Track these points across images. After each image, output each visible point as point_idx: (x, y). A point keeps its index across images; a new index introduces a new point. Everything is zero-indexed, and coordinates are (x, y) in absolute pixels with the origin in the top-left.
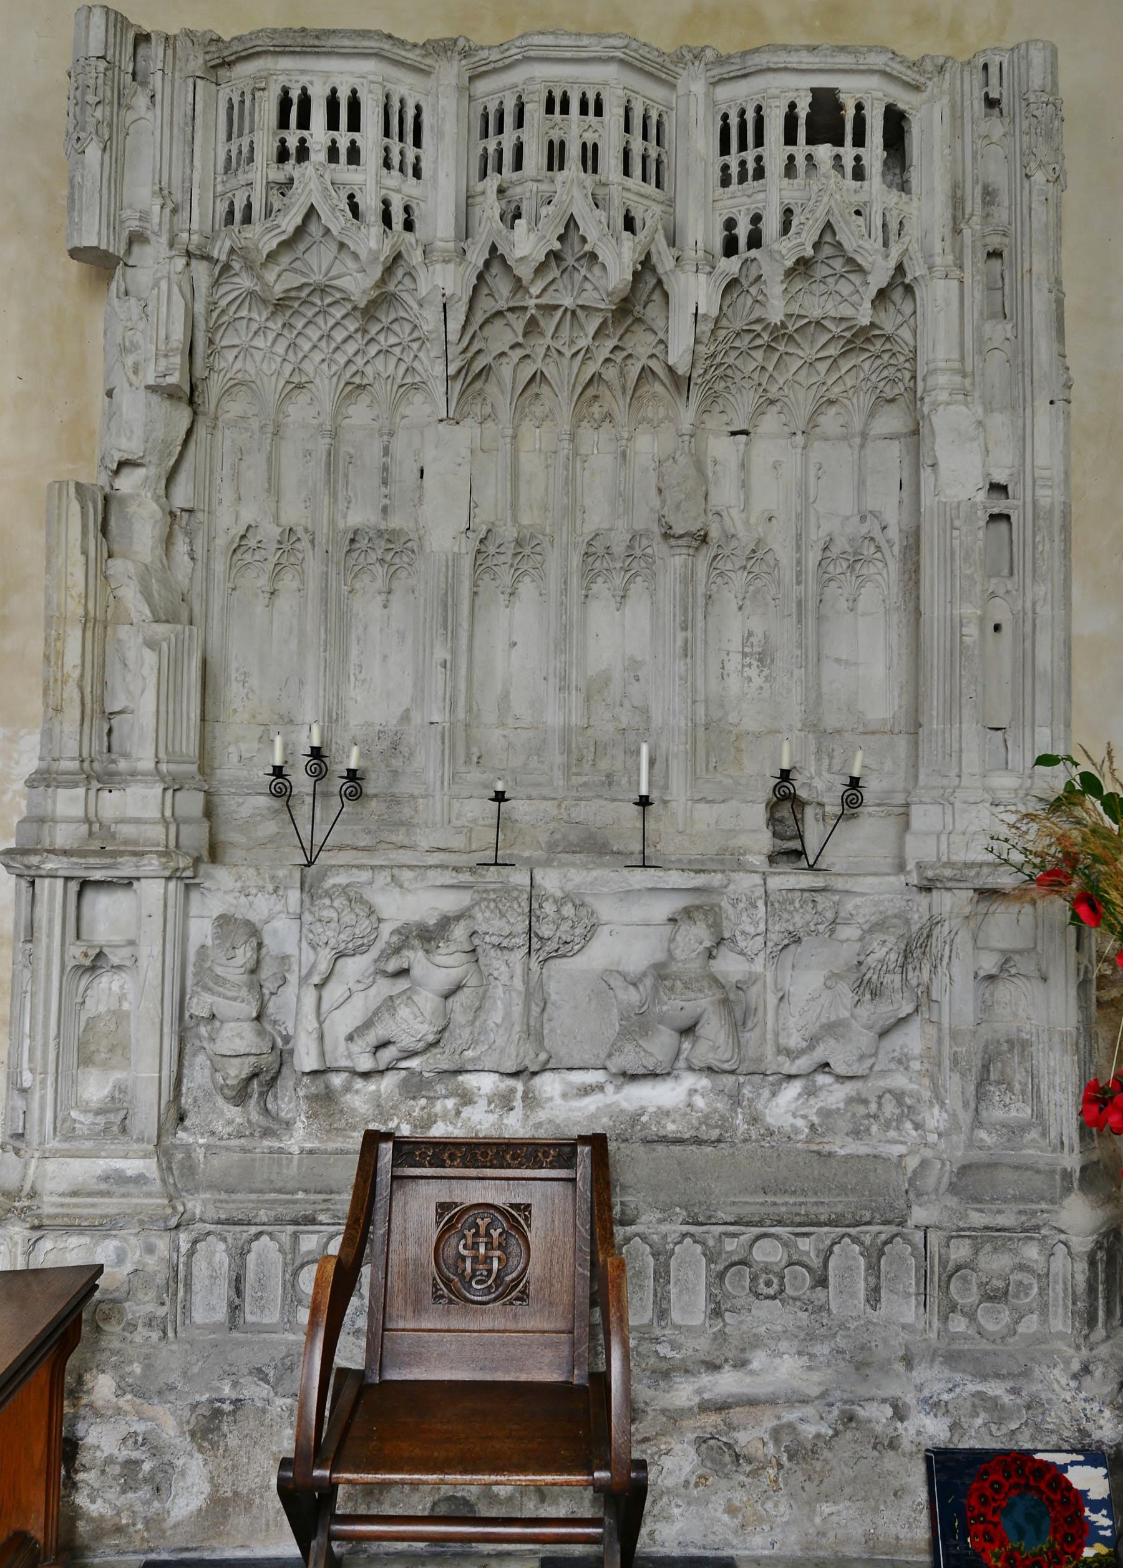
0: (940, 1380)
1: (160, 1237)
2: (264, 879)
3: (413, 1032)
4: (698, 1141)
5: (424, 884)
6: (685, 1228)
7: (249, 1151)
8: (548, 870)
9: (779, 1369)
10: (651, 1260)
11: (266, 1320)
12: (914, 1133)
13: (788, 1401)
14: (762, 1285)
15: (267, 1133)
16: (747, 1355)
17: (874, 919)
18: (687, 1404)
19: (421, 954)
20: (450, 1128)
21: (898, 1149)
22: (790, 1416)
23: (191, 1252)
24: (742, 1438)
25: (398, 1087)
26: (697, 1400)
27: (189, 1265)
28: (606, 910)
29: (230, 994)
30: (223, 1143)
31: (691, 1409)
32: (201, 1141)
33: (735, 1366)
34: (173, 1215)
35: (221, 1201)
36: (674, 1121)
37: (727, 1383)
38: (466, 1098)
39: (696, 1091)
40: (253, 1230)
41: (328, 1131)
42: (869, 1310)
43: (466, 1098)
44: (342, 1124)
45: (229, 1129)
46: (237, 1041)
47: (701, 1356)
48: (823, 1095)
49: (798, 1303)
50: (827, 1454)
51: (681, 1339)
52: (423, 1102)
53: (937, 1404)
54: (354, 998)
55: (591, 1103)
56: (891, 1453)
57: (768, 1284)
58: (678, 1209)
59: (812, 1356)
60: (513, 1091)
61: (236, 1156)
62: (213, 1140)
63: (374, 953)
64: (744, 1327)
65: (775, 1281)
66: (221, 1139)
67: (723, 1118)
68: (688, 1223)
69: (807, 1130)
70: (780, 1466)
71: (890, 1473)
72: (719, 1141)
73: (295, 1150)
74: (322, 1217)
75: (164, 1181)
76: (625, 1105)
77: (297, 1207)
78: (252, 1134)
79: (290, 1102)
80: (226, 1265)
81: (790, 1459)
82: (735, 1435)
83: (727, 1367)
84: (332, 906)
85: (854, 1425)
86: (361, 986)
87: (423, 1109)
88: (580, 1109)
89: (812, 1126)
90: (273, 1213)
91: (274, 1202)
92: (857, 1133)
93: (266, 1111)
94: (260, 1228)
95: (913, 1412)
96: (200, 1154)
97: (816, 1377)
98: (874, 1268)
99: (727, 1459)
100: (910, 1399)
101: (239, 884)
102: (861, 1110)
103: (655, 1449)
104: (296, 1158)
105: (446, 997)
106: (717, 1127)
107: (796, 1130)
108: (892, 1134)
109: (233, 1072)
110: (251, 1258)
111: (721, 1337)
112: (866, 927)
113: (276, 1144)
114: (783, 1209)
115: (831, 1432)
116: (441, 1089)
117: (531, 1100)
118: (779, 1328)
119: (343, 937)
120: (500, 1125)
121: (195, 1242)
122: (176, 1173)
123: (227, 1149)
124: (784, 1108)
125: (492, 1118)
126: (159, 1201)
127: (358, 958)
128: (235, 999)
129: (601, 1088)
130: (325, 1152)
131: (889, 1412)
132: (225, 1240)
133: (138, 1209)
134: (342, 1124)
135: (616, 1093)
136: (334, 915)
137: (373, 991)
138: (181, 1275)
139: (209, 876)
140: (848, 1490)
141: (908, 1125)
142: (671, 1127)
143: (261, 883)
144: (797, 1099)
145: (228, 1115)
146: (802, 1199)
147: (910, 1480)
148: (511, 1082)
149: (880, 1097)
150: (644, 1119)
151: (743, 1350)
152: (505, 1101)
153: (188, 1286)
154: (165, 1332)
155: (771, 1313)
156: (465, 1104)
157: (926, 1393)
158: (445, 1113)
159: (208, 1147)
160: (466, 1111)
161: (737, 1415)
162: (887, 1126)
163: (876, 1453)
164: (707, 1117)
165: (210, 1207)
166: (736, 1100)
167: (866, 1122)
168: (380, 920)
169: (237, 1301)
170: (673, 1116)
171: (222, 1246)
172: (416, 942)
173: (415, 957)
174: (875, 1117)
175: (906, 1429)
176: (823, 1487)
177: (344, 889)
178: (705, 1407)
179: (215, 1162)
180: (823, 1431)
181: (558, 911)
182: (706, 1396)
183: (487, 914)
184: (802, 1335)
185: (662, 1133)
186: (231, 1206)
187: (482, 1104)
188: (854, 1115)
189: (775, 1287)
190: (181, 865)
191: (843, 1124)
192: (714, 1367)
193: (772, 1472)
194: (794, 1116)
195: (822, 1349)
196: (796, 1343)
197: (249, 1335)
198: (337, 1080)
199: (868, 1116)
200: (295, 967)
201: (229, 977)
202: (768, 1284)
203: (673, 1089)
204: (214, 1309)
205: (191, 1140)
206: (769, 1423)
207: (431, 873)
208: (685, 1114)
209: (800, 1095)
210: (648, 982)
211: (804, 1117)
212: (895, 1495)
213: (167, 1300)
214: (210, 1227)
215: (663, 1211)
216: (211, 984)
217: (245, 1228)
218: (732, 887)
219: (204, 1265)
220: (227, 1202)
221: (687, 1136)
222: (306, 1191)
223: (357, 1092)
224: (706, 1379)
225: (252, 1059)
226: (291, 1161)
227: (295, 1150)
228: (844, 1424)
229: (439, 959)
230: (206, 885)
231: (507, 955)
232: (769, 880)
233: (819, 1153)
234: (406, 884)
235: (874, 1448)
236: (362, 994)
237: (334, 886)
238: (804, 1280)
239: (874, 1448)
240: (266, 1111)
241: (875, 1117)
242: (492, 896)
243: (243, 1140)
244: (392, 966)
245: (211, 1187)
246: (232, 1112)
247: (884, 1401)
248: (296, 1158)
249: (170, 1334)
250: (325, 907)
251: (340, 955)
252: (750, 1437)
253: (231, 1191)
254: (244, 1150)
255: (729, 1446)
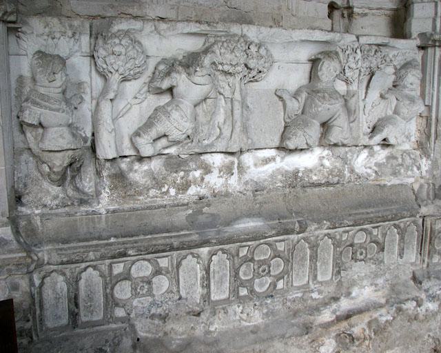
0: (436, 285)
1: (22, 278)
2: (64, 26)
3: (181, 128)
4: (328, 184)
5: (175, 32)
6: (327, 231)
7: (73, 215)
8: (251, 26)
9: (364, 293)
10: (308, 251)
11: (95, 319)
12: (418, 172)
13: (374, 308)
14: (358, 255)
15: (82, 202)
16: (350, 290)
17: (402, 63)
18: (330, 319)
19: (184, 76)
20: (199, 189)
21: (411, 180)
22: (376, 315)
23: (42, 284)
24: (356, 331)
25: (164, 165)
26: (334, 317)
27: (40, 293)
28: (276, 53)
29: (53, 107)
30: (53, 211)
31: (333, 321)
32: (37, 212)
33: (345, 296)
34: (32, 263)
35: (61, 249)
36: (315, 175)
37: (345, 305)
38: (207, 169)
39: (323, 157)
40: (83, 265)
41: (123, 198)
42: (399, 259)
43: (207, 169)
44: (132, 192)
45: (56, 202)
46: (61, 140)
47: (331, 295)
48: (376, 156)
49: (372, 261)
50: (390, 328)
51: (322, 288)
52: (182, 174)
53: (434, 297)
54: (133, 110)
55: (270, 168)
56: (415, 322)
57: (361, 254)
58: (325, 222)
59: (376, 285)
60: (233, 163)
61: (63, 219)
62: (46, 211)
63: (145, 78)
64: (349, 277)
65: (364, 252)
66: (52, 209)
67: (339, 171)
68: (330, 228)
69: (374, 174)
70: (371, 338)
71: (414, 331)
72: (338, 183)
73: (103, 211)
74: (130, 252)
75: (18, 242)
76: (287, 168)
77: (112, 248)
78: (72, 204)
79: (90, 181)
80: (66, 289)
81: (375, 334)
82: (353, 329)
83: (342, 298)
84: (121, 44)
85: (401, 313)
86: (137, 101)
87: (182, 178)
88: (264, 172)
89: (376, 172)
90: (99, 253)
91: (97, 246)
92: (395, 174)
93: (77, 189)
94: (88, 264)
95: (425, 302)
96: (37, 221)
97: (380, 293)
98: (402, 239)
99: (348, 341)
100: (423, 296)
101: (47, 30)
102: (394, 162)
103: (317, 344)
104: (103, 216)
105: (195, 106)
106: (337, 176)
107: (369, 175)
108: (409, 173)
109: (58, 163)
110: (82, 283)
111: (340, 283)
112: (398, 67)
113: (90, 209)
114: (372, 215)
115: (392, 318)
116: (192, 165)
117: (241, 169)
118: (363, 275)
119: (128, 66)
120: (226, 185)
121: (44, 278)
122: (23, 234)
123: (57, 215)
124: (362, 162)
125: (222, 181)
126: (20, 255)
127: (133, 82)
128: (58, 110)
129: (273, 159)
130: (124, 211)
131: (414, 303)
132: (64, 274)
133: (6, 262)
134: (132, 192)
135: (281, 162)
136: (123, 51)
137: (145, 104)
138: (37, 301)
139: (25, 23)
140: (397, 343)
141: (415, 169)
142: (315, 178)
143: (63, 30)
144: (366, 159)
145: (53, 193)
146: (377, 209)
147: (422, 331)
148: (230, 158)
149: (402, 155)
150: (300, 174)
151: (348, 288)
152: (228, 170)
153: (41, 307)
154: (32, 338)
155: (360, 268)
156: (206, 173)
157: (431, 292)
158: (195, 179)
159: (42, 216)
160: (207, 178)
161: (353, 320)
162: (407, 169)
163: (409, 323)
164: (332, 171)
165: (54, 254)
166: (345, 160)
167: (398, 168)
168: (148, 57)
169: (76, 310)
170: (314, 172)
171: (61, 278)
172: (180, 68)
173: (180, 80)
174: (402, 165)
175: (421, 310)
176: (388, 343)
177: (127, 33)
178: (339, 319)
179: (50, 224)
180: (389, 318)
181: (258, 52)
182: (338, 313)
183: (223, 51)
184: (372, 276)
185: (311, 181)
186: (69, 252)
187: (216, 172)
188: (392, 165)
189: (364, 255)
190: (9, 10)
191: (388, 170)
192: (336, 299)
193: (367, 342)
194: (366, 168)
195: (380, 281)
196: (370, 279)
197: (87, 329)
198: (124, 165)
199: (399, 165)
200: (88, 90)
201: (51, 95)
202: (361, 254)
203: (310, 157)
204: (60, 317)
205: (29, 212)
206: (367, 320)
207: (180, 25)
208: (320, 171)
209: (367, 157)
210: (304, 95)
211: (370, 168)
212: (416, 340)
213: (31, 318)
214: (55, 267)
215: (318, 223)
216: (38, 100)
217: (78, 265)
218: (342, 42)
219: (50, 292)
220: (65, 250)
221: (323, 182)
222: (115, 237)
223: (136, 171)
224: (334, 306)
225: (70, 153)
226: (101, 218)
227: (103, 211)
228: (397, 313)
229: (197, 79)
230: (24, 29)
231: (231, 79)
232: (360, 38)
233: (379, 185)
234: (162, 33)
235: (409, 321)
236: (137, 106)
237: (119, 31)
238: (374, 249)
239: (409, 321)
240: (77, 189)
241: (402, 165)
242: (223, 39)
243: (66, 209)
244: (165, 84)
245: (51, 241)
246: (55, 190)
247: (413, 299)
248: (103, 216)
249: (35, 338)
250: (116, 45)
251: (125, 80)
252: (359, 327)
253: (65, 241)
254: (69, 215)
255: (350, 335)
